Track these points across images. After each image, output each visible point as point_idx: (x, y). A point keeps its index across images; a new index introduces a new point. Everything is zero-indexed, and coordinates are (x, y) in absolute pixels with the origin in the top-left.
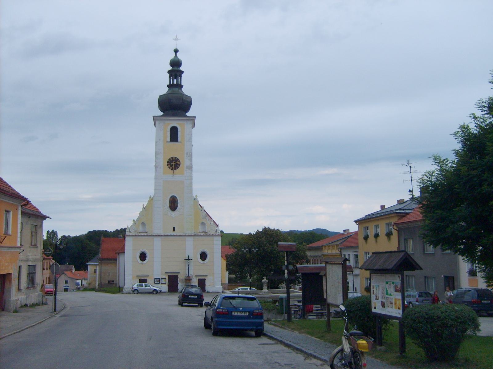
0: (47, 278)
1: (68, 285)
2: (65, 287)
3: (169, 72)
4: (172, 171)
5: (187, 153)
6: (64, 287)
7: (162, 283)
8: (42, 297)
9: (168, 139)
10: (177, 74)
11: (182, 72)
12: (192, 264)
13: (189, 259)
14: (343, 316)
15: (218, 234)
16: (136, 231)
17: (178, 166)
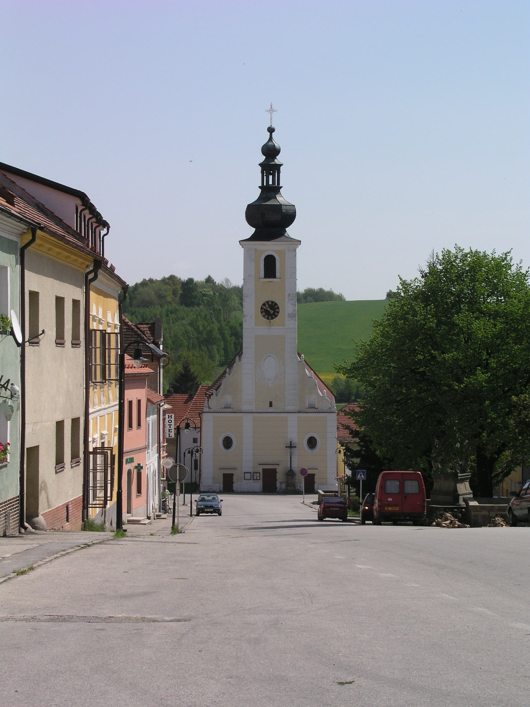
5: (289, 295)
7: (250, 474)
8: (201, 428)
17: (270, 303)
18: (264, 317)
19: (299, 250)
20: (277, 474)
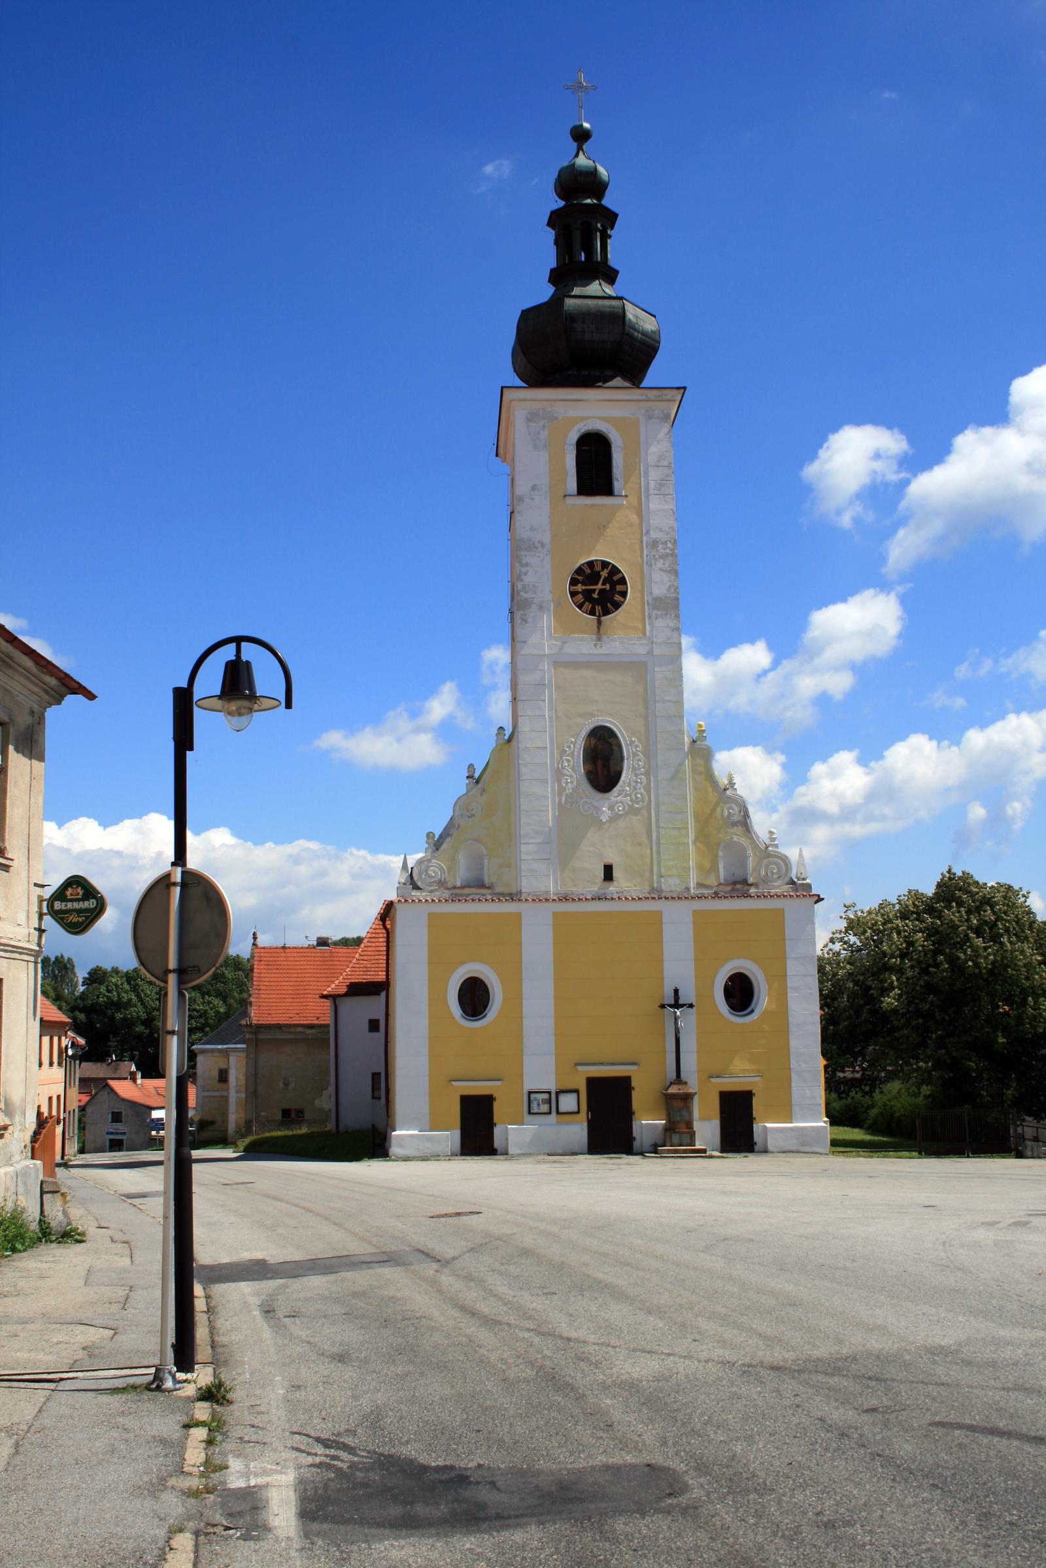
0: (50, 1099)
1: (120, 1127)
2: (112, 1133)
6: (108, 1133)
7: (574, 1096)
8: (42, 1193)
9: (572, 484)
13: (681, 1002)
18: (580, 607)
20: (634, 1094)
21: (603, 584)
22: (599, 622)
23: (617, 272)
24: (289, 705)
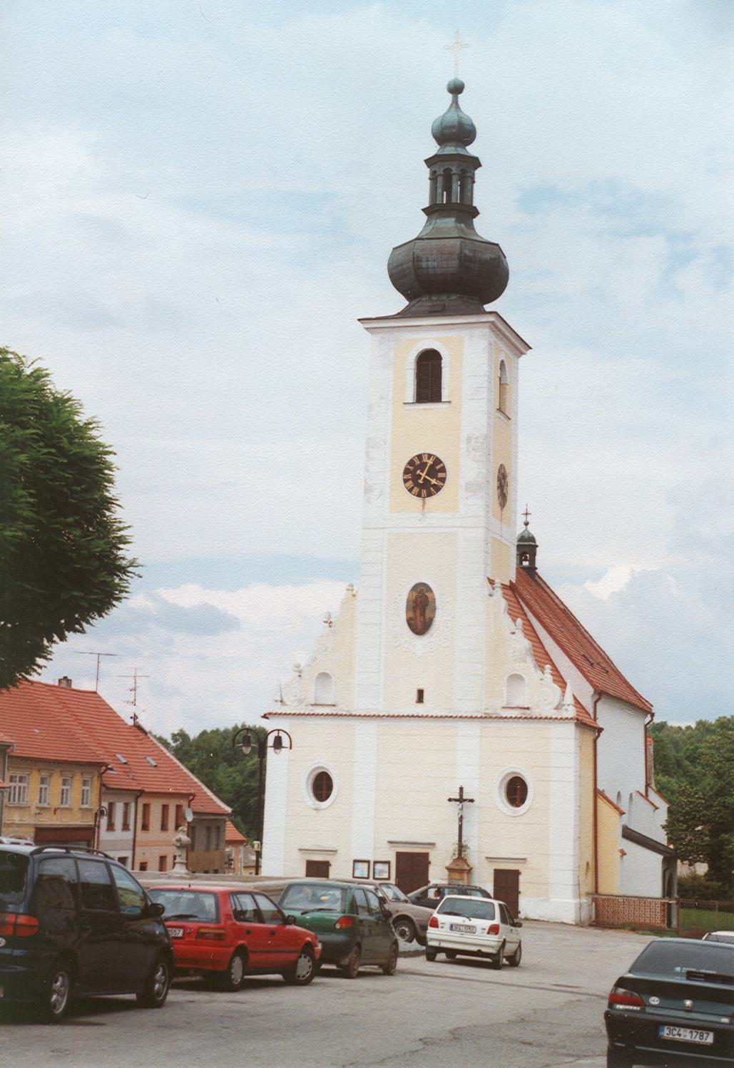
3: (429, 162)
4: (418, 501)
7: (366, 865)
10: (451, 170)
11: (476, 163)
12: (472, 814)
14: (450, 150)
15: (565, 715)
16: (300, 702)
18: (410, 490)
19: (478, 173)
21: (425, 479)
22: (424, 503)
23: (479, 213)
24: (291, 748)
